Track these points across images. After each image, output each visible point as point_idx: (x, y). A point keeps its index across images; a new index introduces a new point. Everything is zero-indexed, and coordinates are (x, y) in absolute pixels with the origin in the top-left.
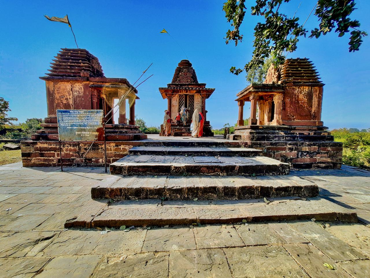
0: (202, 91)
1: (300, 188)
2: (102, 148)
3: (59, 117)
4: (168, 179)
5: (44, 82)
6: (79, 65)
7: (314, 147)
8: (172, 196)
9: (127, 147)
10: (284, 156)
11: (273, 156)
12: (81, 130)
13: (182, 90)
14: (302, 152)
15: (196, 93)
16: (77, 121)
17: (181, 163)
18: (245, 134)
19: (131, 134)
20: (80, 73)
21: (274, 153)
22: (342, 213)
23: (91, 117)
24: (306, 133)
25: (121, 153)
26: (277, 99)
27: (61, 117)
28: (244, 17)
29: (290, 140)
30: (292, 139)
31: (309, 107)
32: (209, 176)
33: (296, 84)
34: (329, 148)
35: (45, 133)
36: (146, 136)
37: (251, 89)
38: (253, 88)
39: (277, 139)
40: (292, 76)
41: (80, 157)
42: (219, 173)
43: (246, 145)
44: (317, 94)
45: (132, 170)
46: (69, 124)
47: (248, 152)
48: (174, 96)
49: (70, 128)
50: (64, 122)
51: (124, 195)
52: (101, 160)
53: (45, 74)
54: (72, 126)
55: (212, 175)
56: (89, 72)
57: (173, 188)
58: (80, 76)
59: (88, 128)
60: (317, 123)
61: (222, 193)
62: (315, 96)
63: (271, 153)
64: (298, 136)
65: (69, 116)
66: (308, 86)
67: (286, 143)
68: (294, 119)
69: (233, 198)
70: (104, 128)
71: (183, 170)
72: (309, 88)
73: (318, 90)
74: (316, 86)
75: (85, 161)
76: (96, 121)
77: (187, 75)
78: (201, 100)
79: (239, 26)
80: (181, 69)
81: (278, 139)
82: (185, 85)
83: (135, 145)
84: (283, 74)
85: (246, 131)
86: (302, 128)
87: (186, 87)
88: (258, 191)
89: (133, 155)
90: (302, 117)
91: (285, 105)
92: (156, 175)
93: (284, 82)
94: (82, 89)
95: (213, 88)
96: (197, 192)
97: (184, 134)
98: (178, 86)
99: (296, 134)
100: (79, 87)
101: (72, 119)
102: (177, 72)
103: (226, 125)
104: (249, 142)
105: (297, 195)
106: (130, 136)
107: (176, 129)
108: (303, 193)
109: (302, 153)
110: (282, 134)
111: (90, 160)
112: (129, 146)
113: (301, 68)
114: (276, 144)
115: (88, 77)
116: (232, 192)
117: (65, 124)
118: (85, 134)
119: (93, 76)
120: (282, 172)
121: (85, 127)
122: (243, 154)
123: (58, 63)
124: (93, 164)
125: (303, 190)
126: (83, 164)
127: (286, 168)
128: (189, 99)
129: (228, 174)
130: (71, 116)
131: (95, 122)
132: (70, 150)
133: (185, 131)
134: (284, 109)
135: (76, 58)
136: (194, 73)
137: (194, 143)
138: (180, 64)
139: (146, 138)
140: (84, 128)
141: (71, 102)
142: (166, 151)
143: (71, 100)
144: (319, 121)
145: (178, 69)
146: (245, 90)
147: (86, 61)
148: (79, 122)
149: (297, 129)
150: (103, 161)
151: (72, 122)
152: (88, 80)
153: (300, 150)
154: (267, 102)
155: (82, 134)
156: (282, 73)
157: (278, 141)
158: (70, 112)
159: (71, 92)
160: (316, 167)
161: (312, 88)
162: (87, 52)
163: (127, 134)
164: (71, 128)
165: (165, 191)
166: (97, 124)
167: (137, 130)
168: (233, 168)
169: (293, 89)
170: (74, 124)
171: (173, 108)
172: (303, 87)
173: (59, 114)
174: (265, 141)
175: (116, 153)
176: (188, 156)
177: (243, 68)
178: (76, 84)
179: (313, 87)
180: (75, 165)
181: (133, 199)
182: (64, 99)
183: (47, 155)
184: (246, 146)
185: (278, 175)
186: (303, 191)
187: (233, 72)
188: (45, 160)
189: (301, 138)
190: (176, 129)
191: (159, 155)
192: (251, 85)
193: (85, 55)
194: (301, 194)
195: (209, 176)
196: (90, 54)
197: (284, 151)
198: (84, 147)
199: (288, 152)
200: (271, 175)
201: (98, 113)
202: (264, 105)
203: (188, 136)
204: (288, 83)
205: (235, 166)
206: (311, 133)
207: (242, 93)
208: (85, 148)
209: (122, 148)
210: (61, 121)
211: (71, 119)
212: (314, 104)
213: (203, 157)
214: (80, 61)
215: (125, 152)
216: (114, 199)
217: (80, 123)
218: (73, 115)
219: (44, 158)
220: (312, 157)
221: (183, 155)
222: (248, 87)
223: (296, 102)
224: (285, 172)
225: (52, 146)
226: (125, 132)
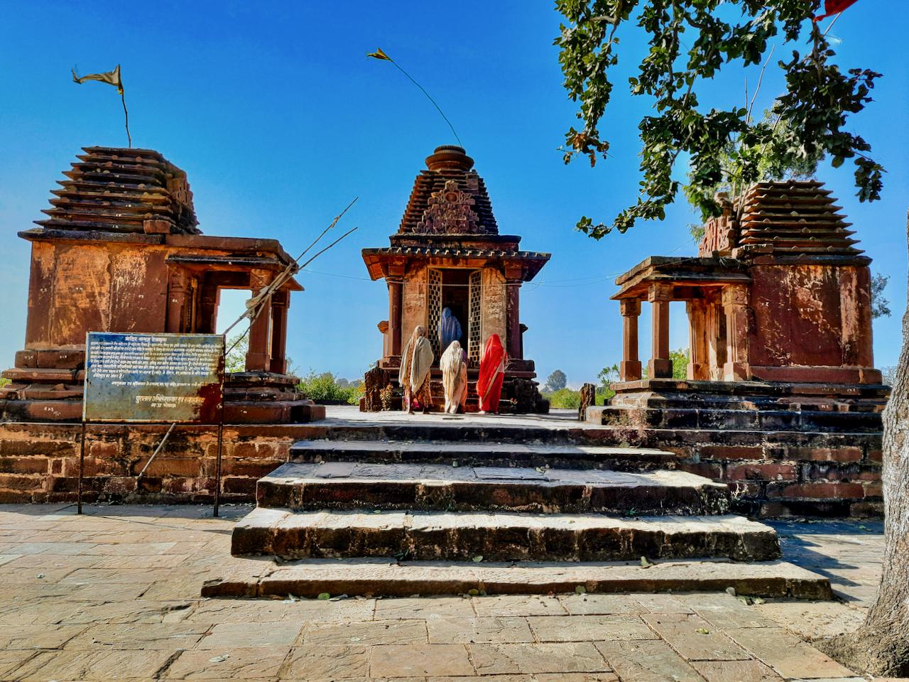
0: (507, 261)
1: (733, 538)
2: (196, 446)
3: (92, 353)
4: (410, 516)
5: (28, 244)
6: (138, 196)
7: (849, 448)
8: (422, 550)
9: (275, 444)
10: (757, 475)
12: (154, 391)
13: (441, 258)
14: (812, 463)
15: (486, 266)
16: (144, 366)
17: (444, 478)
18: (635, 404)
19: (284, 403)
20: (141, 221)
21: (724, 466)
22: (797, 580)
23: (187, 354)
24: (825, 405)
25: (256, 460)
26: (732, 300)
27: (97, 352)
28: (607, 106)
29: (775, 427)
30: (780, 423)
31: (832, 326)
32: (516, 512)
33: (785, 258)
35: (16, 398)
36: (323, 412)
37: (650, 274)
38: (656, 269)
39: (732, 422)
40: (771, 235)
41: (125, 474)
42: (539, 506)
43: (632, 437)
44: (853, 289)
45: (316, 495)
46: (118, 374)
47: (634, 458)
48: (412, 277)
49: (120, 383)
50: (105, 366)
51: (308, 545)
52: (189, 484)
53: (34, 222)
54: (127, 378)
55: (523, 511)
56: (168, 218)
57: (426, 530)
58: (142, 231)
59: (173, 384)
60: (861, 374)
61: (541, 543)
62: (847, 293)
63: (715, 466)
64: (799, 413)
65: (121, 351)
66: (823, 264)
67: (759, 437)
68: (787, 362)
69: (568, 558)
70: (220, 384)
71: (447, 495)
72: (824, 271)
73: (854, 276)
74: (847, 265)
75: (138, 485)
76: (200, 364)
77: (455, 199)
78: (505, 291)
79: (595, 122)
80: (437, 177)
81: (737, 422)
82: (451, 240)
83: (298, 436)
84: (745, 228)
85: (640, 396)
86: (811, 390)
87: (453, 248)
88: (629, 542)
89: (301, 463)
90: (809, 355)
91: (755, 319)
92: (377, 509)
93: (745, 252)
94: (143, 266)
95: (544, 252)
96: (482, 542)
98: (427, 243)
99: (794, 407)
100: (132, 263)
101: (131, 358)
103: (606, 371)
104: (640, 428)
105: (727, 555)
106: (281, 407)
108: (741, 550)
109: (813, 468)
110: (749, 406)
111: (156, 482)
112: (281, 441)
113: (799, 211)
114: (724, 438)
115: (164, 234)
116: (565, 543)
117: (108, 373)
118: (163, 402)
119: (177, 232)
121: (167, 381)
122: (618, 463)
123: (73, 191)
124: (163, 494)
125: (740, 542)
126: (131, 497)
127: (719, 496)
129: (563, 508)
130: (128, 351)
131: (196, 368)
132: (97, 452)
134: (754, 331)
135: (129, 176)
136: (482, 189)
137: (476, 432)
138: (431, 161)
139: (321, 417)
140: (162, 384)
141: (104, 304)
142: (397, 452)
143: (104, 299)
144: (867, 368)
145: (425, 178)
146: (635, 272)
147: (157, 185)
148: (150, 367)
149: (796, 392)
150: (197, 486)
151: (130, 367)
152: (163, 242)
153: (806, 458)
154: (712, 305)
155: (155, 402)
156: (744, 224)
158: (127, 339)
159: (107, 276)
160: (864, 511)
161: (834, 271)
162: (158, 157)
163: (272, 403)
164: (124, 383)
165: (405, 536)
166: (202, 373)
167: (294, 391)
168: (577, 491)
169: (778, 271)
170: (134, 372)
171: (407, 317)
172: (808, 268)
173: (92, 343)
174: (695, 427)
175: (238, 460)
176: (459, 466)
177: (610, 223)
178: (125, 252)
179: (838, 268)
180: (106, 500)
181: (330, 555)
182: (84, 294)
183: (22, 467)
184: (634, 441)
185: (700, 514)
186: (742, 545)
187: (585, 230)
188: (13, 483)
189: (809, 420)
191: (376, 463)
192: (649, 262)
193: (157, 169)
194: (738, 553)
196: (167, 163)
198: (143, 442)
200: (679, 515)
201: (207, 343)
202: (705, 313)
204: (756, 255)
205: (581, 486)
206: (840, 405)
207: (630, 279)
208: (146, 443)
209: (260, 446)
210: (96, 364)
211: (127, 357)
212: (846, 317)
213: (502, 469)
214: (141, 186)
215: (267, 459)
216: (285, 557)
217: (151, 370)
218: (134, 349)
219: (12, 475)
220: (845, 480)
221: (445, 463)
222: (643, 266)
223: (790, 312)
224: (716, 507)
225: (42, 439)
226: (267, 397)
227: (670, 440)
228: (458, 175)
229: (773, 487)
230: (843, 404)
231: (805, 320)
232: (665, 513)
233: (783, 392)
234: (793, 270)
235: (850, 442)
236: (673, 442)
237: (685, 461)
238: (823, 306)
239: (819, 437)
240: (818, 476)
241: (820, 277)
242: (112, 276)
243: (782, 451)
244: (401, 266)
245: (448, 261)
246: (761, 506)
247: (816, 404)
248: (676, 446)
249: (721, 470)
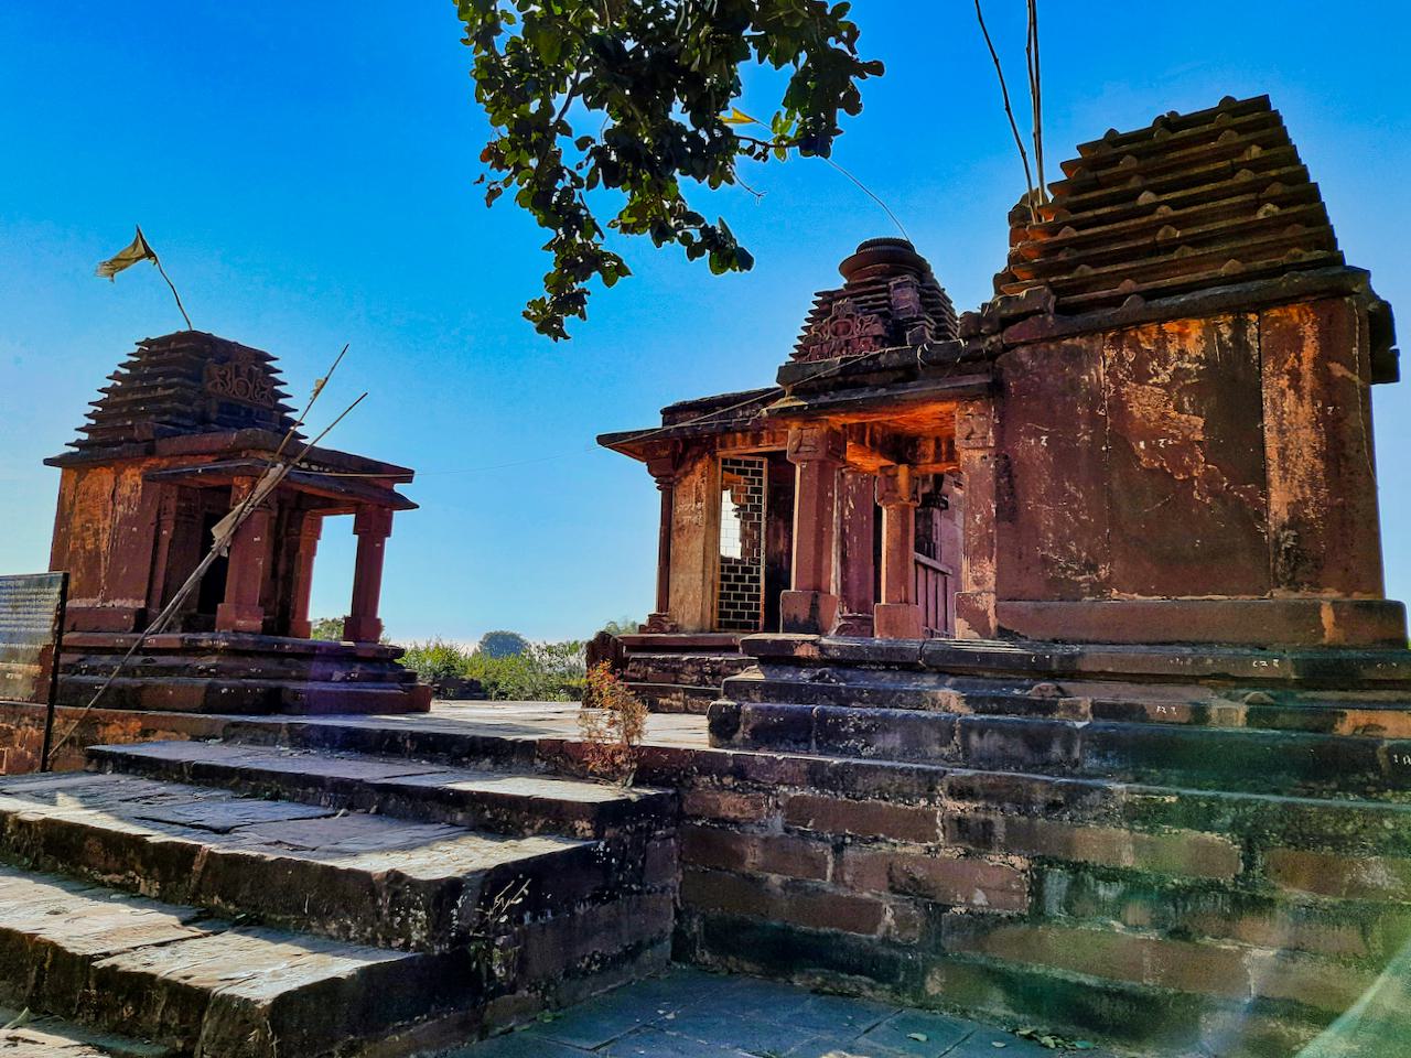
11: (829, 872)
14: (1076, 868)
21: (838, 849)
24: (1165, 706)
30: (1018, 748)
34: (1367, 866)
39: (893, 741)
44: (1306, 367)
48: (686, 474)
60: (1327, 616)
62: (1284, 382)
63: (817, 848)
67: (929, 782)
68: (1099, 589)
72: (1210, 331)
73: (1309, 331)
90: (1175, 569)
97: (667, 701)
99: (1074, 710)
107: (650, 669)
109: (1077, 885)
120: (389, 926)
122: (488, 814)
133: (695, 678)
157: (903, 756)
161: (1239, 327)
169: (1074, 356)
189: (1104, 744)
195: (103, 884)
197: (920, 839)
199: (951, 853)
203: (687, 711)
212: (1282, 453)
220: (1181, 934)
227: (721, 775)
228: (873, 287)
229: (958, 925)
230: (1227, 704)
231: (1151, 471)
232: (309, 927)
233: (1055, 666)
234: (1116, 343)
235: (1202, 818)
236: (728, 780)
237: (750, 828)
238: (1204, 430)
239: (1097, 795)
240: (1092, 908)
241: (1194, 348)
242: (114, 504)
243: (988, 824)
244: (667, 457)
245: (744, 439)
246: (925, 972)
247: (1139, 701)
248: (735, 790)
249: (830, 858)
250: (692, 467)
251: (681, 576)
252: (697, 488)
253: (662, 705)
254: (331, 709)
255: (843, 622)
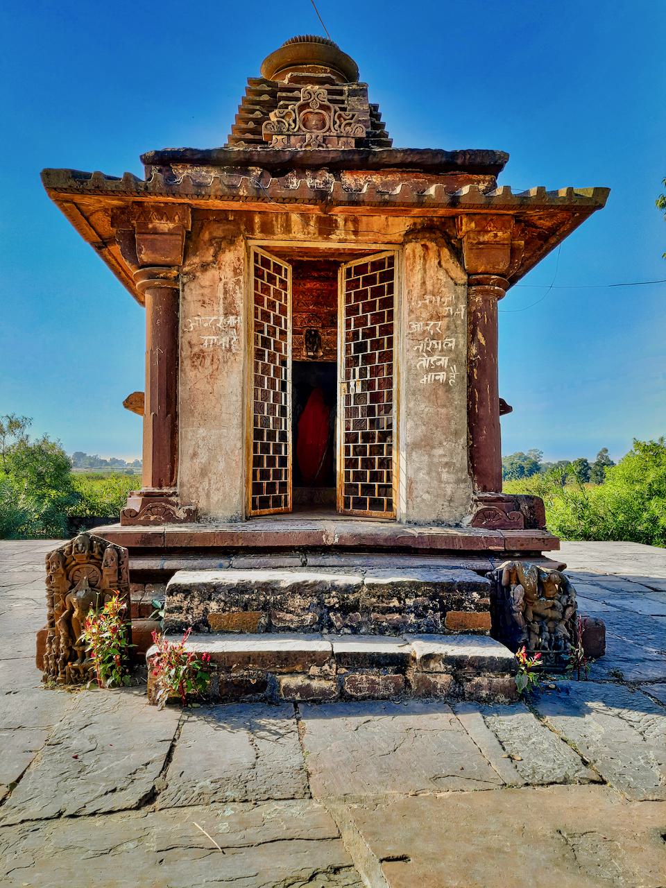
48: (205, 267)
78: (462, 307)
97: (298, 681)
102: (252, 112)
128: (348, 297)
133: (309, 617)
190: (214, 606)
250: (215, 256)
251: (202, 432)
252: (226, 292)
253: (288, 690)
254: (603, 192)
255: (482, 506)
